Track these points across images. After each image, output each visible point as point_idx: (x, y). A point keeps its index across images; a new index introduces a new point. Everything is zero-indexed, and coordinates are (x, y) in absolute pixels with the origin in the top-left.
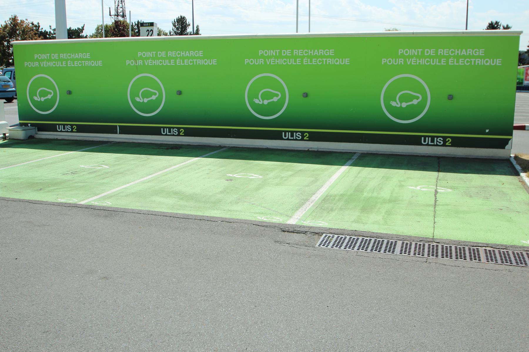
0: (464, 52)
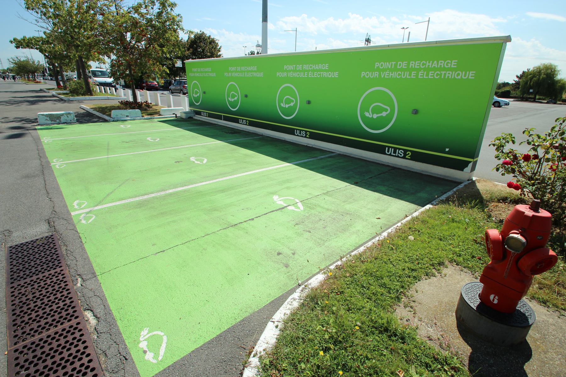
0: (435, 64)
